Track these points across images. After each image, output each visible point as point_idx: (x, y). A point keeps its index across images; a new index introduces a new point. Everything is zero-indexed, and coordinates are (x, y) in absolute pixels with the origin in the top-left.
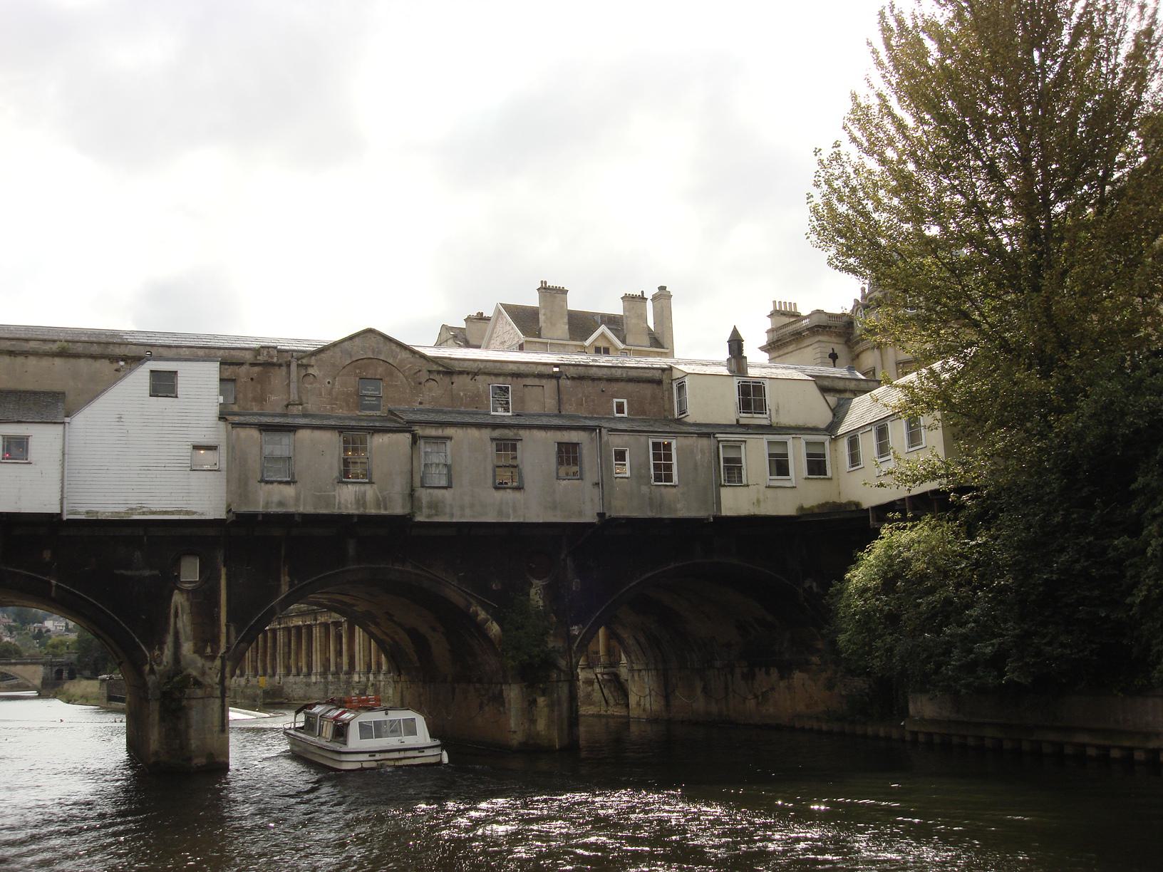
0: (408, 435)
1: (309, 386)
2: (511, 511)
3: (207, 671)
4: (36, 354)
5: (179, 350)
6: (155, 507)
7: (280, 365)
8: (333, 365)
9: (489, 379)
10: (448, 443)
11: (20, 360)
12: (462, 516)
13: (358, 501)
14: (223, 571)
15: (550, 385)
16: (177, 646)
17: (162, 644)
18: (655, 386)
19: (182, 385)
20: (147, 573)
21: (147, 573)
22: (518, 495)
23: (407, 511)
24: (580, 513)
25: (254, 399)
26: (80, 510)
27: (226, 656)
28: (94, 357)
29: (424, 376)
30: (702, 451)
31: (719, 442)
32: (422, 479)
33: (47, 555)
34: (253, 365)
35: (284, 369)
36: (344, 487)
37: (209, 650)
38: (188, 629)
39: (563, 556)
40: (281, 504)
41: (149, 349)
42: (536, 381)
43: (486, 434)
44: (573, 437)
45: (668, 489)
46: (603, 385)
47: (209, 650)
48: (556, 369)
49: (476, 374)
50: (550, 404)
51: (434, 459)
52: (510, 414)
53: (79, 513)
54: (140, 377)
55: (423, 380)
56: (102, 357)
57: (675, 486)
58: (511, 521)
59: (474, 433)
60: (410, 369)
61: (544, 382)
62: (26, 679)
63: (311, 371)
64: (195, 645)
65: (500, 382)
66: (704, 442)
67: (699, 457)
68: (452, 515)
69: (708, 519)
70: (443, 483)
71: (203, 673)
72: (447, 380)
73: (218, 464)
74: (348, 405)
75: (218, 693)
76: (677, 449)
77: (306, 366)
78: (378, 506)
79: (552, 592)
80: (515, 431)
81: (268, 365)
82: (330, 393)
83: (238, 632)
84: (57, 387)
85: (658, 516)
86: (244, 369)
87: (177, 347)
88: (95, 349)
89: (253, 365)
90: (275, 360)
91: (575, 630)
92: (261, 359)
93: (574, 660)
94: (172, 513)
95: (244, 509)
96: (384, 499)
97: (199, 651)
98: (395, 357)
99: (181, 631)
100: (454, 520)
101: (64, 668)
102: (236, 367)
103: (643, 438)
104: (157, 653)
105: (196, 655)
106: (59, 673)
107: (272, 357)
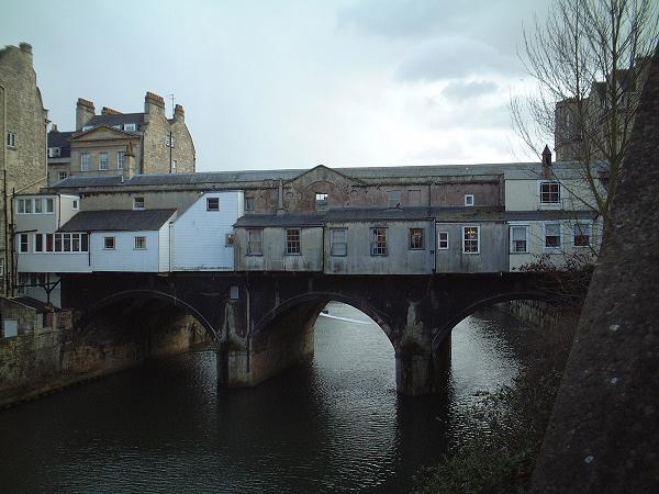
20: (215, 294)
21: (215, 294)
23: (319, 270)
32: (332, 252)
38: (233, 322)
40: (256, 267)
42: (417, 188)
43: (368, 225)
46: (459, 187)
54: (203, 202)
66: (500, 226)
72: (363, 190)
77: (288, 188)
78: (305, 267)
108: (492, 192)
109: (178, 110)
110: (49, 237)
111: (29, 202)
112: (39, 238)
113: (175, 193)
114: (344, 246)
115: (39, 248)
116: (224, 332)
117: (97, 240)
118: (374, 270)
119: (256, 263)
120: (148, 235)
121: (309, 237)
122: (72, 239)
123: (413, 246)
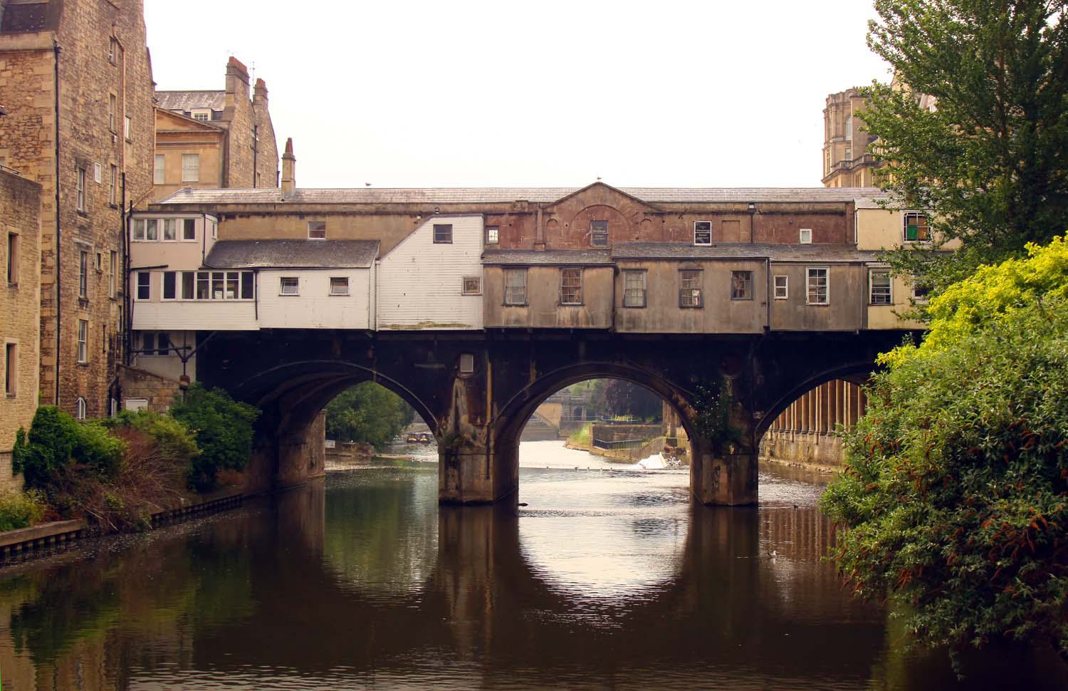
0: (611, 270)
1: (552, 229)
2: (692, 325)
3: (478, 435)
4: (360, 213)
5: (459, 206)
6: (437, 322)
7: (531, 214)
8: (570, 211)
9: (693, 217)
10: (645, 273)
11: (350, 218)
12: (653, 328)
13: (572, 318)
14: (489, 365)
15: (744, 220)
16: (457, 417)
17: (447, 416)
18: (838, 217)
19: (456, 234)
20: (436, 366)
21: (436, 366)
22: (699, 313)
23: (609, 325)
24: (750, 326)
25: (512, 240)
26: (387, 324)
27: (491, 425)
28: (400, 214)
29: (641, 217)
30: (854, 278)
31: (869, 269)
32: (624, 301)
33: (370, 354)
34: (511, 214)
35: (534, 216)
36: (563, 309)
37: (479, 421)
38: (465, 407)
39: (750, 358)
40: (517, 321)
41: (437, 206)
42: (733, 217)
43: (675, 266)
44: (747, 266)
45: (821, 308)
46: (790, 219)
47: (479, 421)
48: (752, 207)
49: (683, 214)
50: (745, 234)
51: (634, 285)
52: (710, 244)
53: (386, 326)
54: (427, 229)
55: (640, 220)
56: (405, 213)
57: (827, 306)
58: (692, 332)
59: (666, 265)
60: (629, 212)
61: (740, 217)
62: (545, 418)
63: (553, 217)
64: (470, 417)
65: (702, 219)
66: (856, 269)
67: (850, 282)
68: (646, 328)
69: (855, 332)
70: (641, 303)
71: (474, 437)
72: (658, 219)
73: (702, 219)
74: (581, 241)
75: (485, 452)
76: (831, 275)
77: (550, 214)
78: (588, 323)
79: (740, 386)
80: (698, 263)
81: (521, 214)
82: (567, 234)
83: (499, 409)
84: (376, 238)
85: (812, 330)
86: (504, 218)
87: (457, 204)
88: (401, 208)
89: (511, 214)
90: (526, 210)
91: (758, 415)
92: (517, 210)
93: (756, 440)
94: (449, 326)
95: (492, 325)
96: (592, 317)
97: (472, 421)
98: (618, 204)
99: (460, 408)
100: (648, 332)
101: (583, 407)
102: (499, 217)
103: (800, 269)
104: (443, 422)
105: (470, 425)
106: (578, 412)
107: (524, 208)
108: (837, 226)
109: (261, 87)
110: (188, 277)
111: (155, 221)
112: (170, 278)
113: (376, 218)
114: (641, 294)
115: (170, 293)
116: (451, 420)
117: (268, 283)
118: (684, 326)
119: (512, 317)
120: (358, 279)
121: (596, 281)
122: (210, 280)
123: (737, 294)
